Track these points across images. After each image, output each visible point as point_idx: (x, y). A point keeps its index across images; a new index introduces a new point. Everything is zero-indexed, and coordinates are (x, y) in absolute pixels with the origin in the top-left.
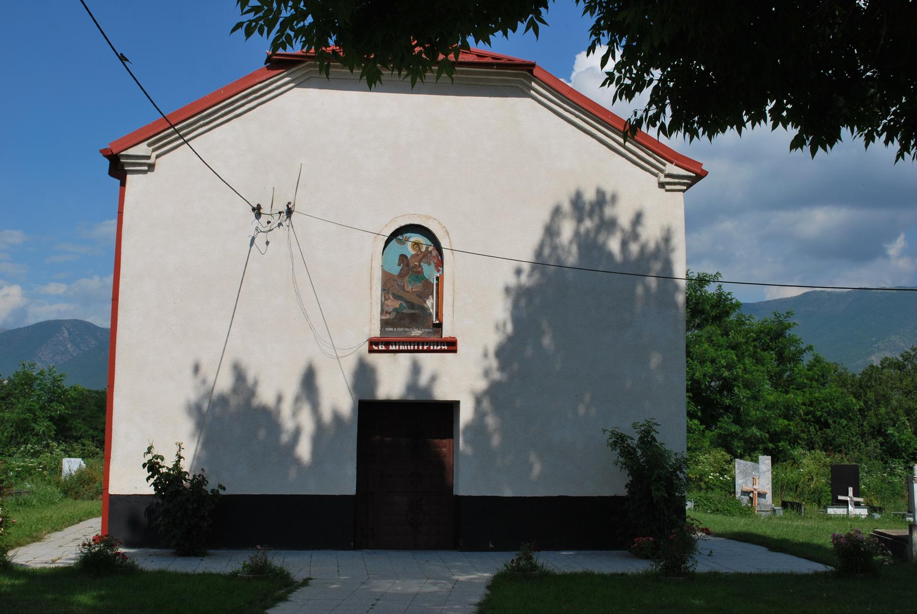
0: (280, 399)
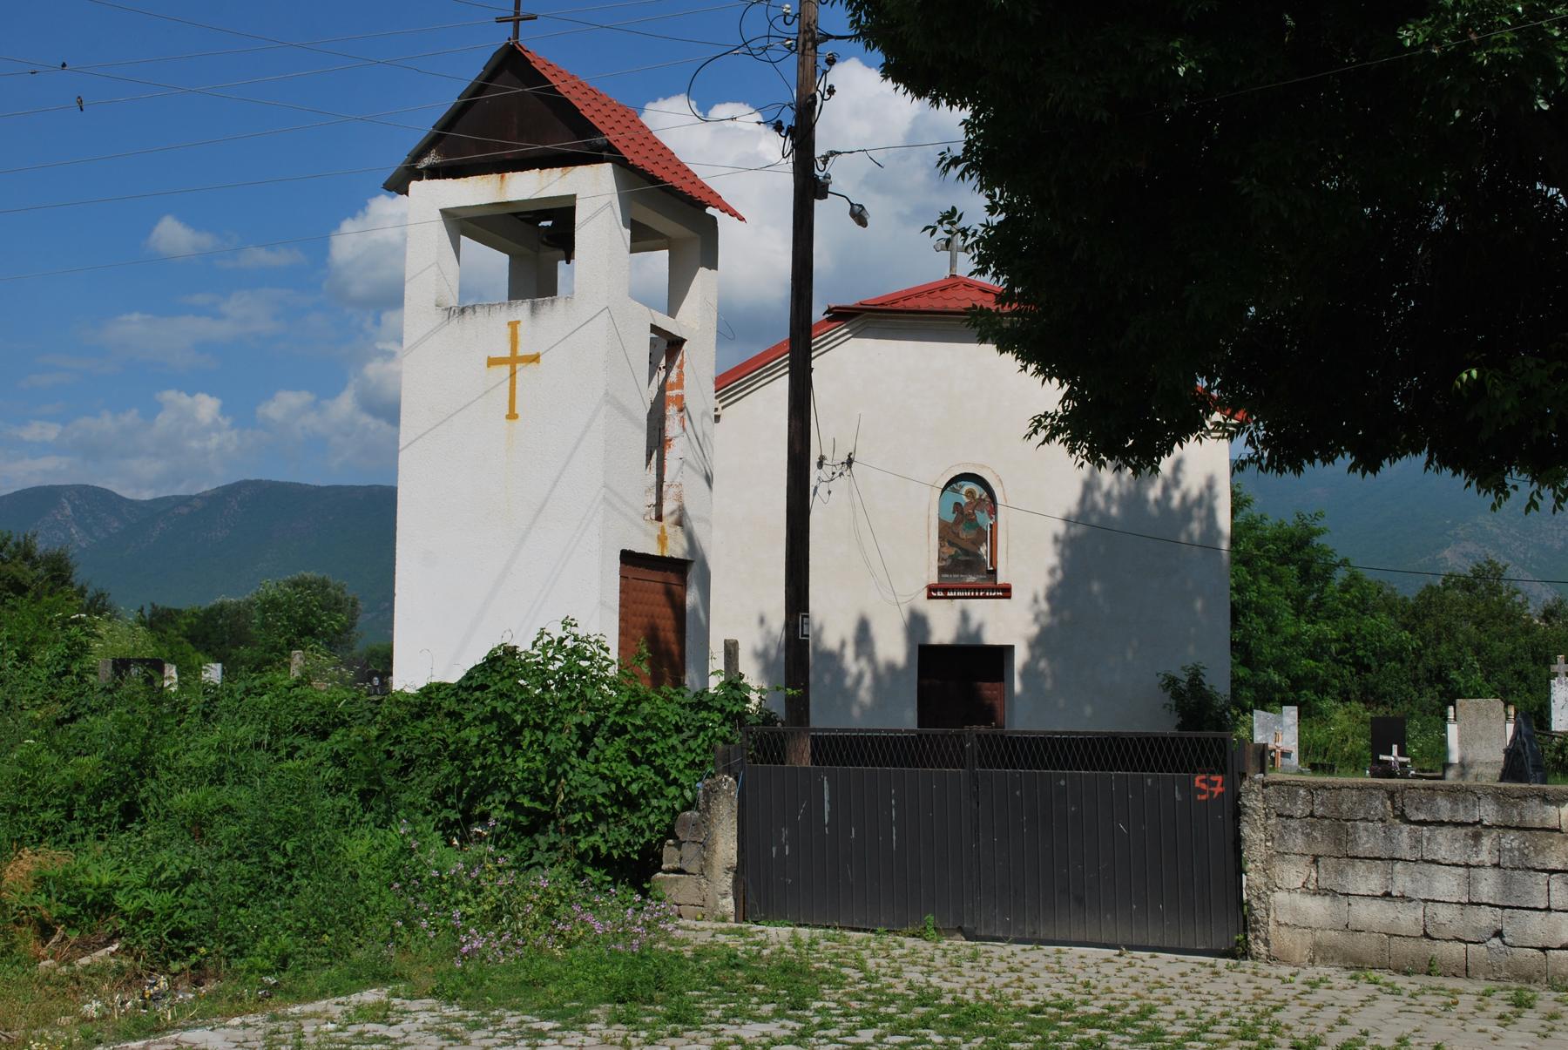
0: (843, 644)
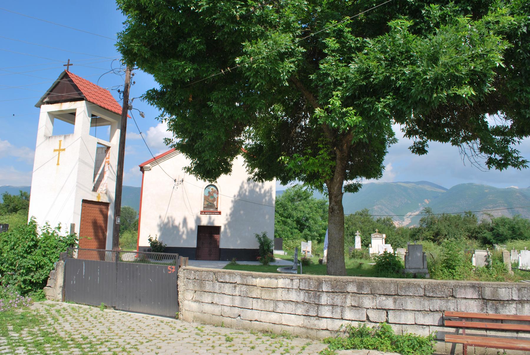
0: (180, 224)
